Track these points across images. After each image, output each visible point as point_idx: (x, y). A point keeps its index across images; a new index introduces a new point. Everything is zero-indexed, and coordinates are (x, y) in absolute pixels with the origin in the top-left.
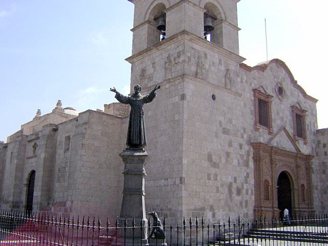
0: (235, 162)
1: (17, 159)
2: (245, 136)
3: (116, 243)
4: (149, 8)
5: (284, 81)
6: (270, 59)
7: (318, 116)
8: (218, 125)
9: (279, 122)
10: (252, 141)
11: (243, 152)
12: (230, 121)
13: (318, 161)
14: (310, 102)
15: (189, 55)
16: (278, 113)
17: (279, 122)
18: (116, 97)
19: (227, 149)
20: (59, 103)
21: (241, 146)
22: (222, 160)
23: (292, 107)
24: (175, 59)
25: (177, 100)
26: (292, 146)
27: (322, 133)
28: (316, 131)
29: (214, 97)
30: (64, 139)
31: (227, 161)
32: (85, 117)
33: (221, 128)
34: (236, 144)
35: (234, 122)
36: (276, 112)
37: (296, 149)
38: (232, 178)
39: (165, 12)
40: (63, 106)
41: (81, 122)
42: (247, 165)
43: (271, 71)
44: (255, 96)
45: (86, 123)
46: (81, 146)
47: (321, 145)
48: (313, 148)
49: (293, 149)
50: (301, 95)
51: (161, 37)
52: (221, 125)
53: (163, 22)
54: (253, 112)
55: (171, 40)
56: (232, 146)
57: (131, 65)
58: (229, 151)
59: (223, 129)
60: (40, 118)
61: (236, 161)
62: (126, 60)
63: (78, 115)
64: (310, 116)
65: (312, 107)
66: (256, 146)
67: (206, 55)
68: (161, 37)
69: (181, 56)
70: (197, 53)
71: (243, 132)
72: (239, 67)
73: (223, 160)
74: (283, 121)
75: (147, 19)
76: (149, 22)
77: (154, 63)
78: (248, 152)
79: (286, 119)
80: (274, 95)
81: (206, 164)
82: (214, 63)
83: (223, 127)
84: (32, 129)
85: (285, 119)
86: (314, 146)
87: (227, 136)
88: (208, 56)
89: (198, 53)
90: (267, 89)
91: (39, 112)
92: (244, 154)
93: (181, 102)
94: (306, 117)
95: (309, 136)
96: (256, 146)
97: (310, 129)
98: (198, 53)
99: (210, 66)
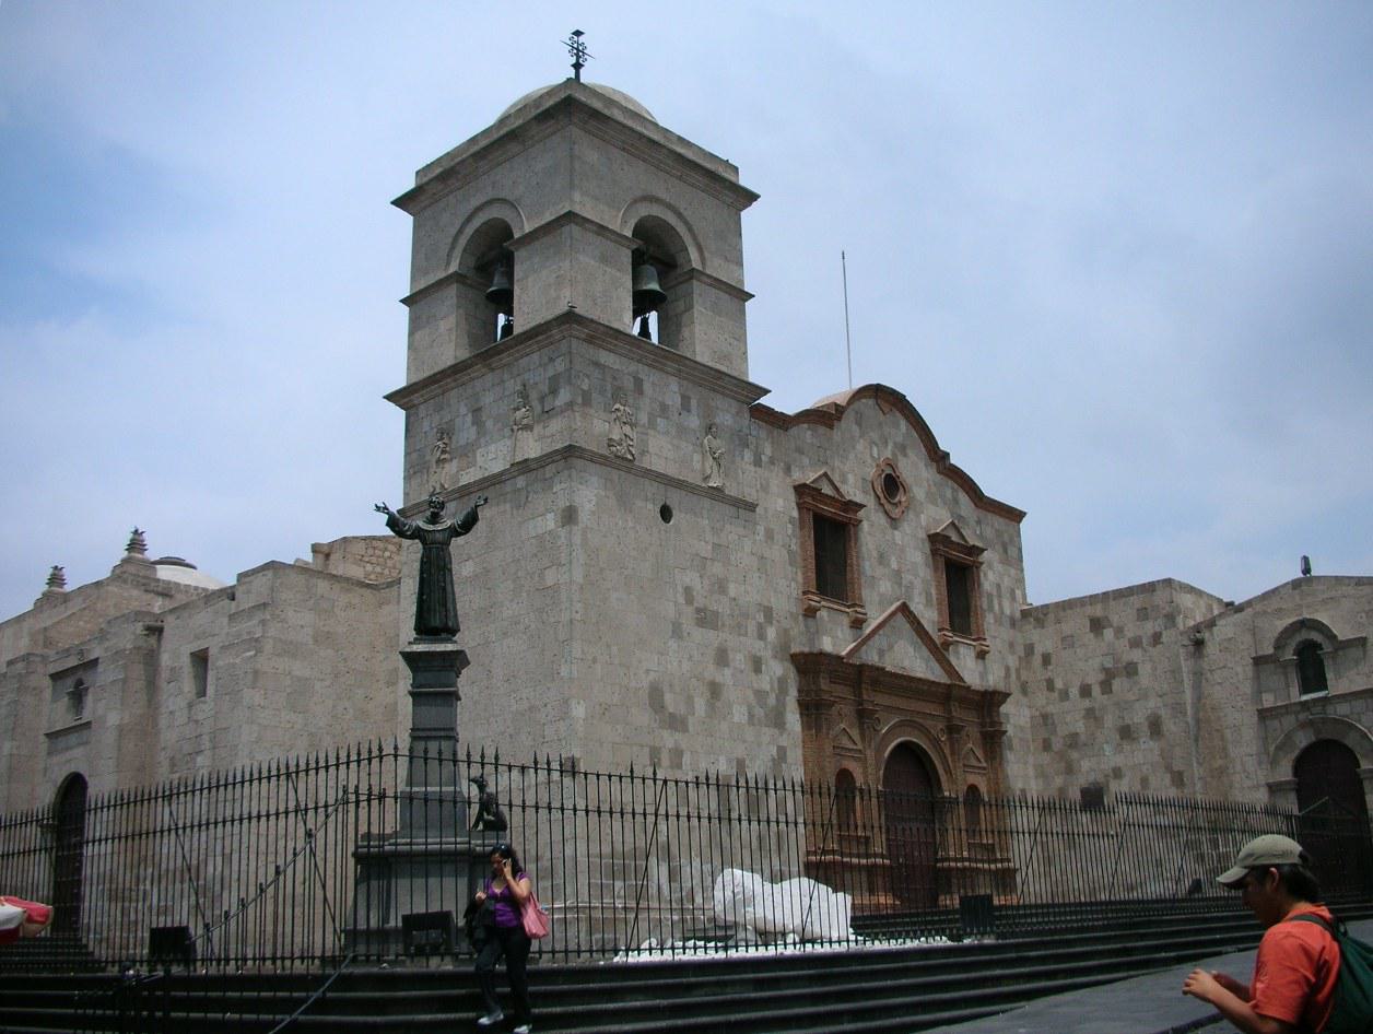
0: (739, 715)
2: (771, 633)
3: (426, 838)
4: (460, 231)
6: (859, 384)
7: (1026, 564)
8: (681, 600)
9: (885, 586)
10: (795, 649)
11: (765, 682)
12: (721, 586)
13: (1027, 712)
14: (998, 522)
15: (585, 387)
16: (882, 559)
17: (885, 586)
18: (387, 525)
19: (711, 672)
20: (136, 544)
21: (757, 665)
22: (697, 706)
23: (934, 539)
24: (542, 399)
25: (551, 525)
26: (936, 666)
27: (1037, 620)
30: (186, 661)
31: (711, 707)
32: (261, 583)
33: (690, 610)
34: (739, 656)
35: (732, 590)
36: (875, 554)
37: (947, 672)
38: (729, 761)
39: (512, 248)
40: (152, 554)
41: (245, 601)
42: (778, 722)
43: (859, 424)
44: (800, 506)
45: (265, 605)
46: (250, 677)
47: (1037, 660)
48: (1007, 669)
49: (934, 673)
50: (963, 498)
51: (502, 320)
52: (689, 600)
53: (505, 280)
54: (799, 559)
55: (531, 338)
56: (727, 665)
57: (403, 413)
58: (719, 679)
59: (698, 610)
60: (66, 597)
61: (744, 709)
62: (389, 397)
63: (233, 582)
65: (1006, 538)
66: (810, 665)
68: (502, 320)
69: (562, 391)
70: (609, 379)
71: (762, 620)
72: (747, 415)
73: (700, 705)
74: (900, 585)
75: (453, 268)
76: (457, 278)
77: (479, 409)
78: (782, 682)
79: (910, 577)
80: (870, 501)
81: (643, 717)
82: (664, 408)
83: (696, 605)
84: (41, 637)
85: (907, 578)
86: (1012, 661)
87: (712, 634)
88: (647, 386)
89: (614, 378)
90: (844, 481)
91: (56, 578)
92: (768, 688)
93: (562, 532)
94: (984, 567)
95: (996, 634)
96: (810, 665)
97: (996, 607)
98: (614, 378)
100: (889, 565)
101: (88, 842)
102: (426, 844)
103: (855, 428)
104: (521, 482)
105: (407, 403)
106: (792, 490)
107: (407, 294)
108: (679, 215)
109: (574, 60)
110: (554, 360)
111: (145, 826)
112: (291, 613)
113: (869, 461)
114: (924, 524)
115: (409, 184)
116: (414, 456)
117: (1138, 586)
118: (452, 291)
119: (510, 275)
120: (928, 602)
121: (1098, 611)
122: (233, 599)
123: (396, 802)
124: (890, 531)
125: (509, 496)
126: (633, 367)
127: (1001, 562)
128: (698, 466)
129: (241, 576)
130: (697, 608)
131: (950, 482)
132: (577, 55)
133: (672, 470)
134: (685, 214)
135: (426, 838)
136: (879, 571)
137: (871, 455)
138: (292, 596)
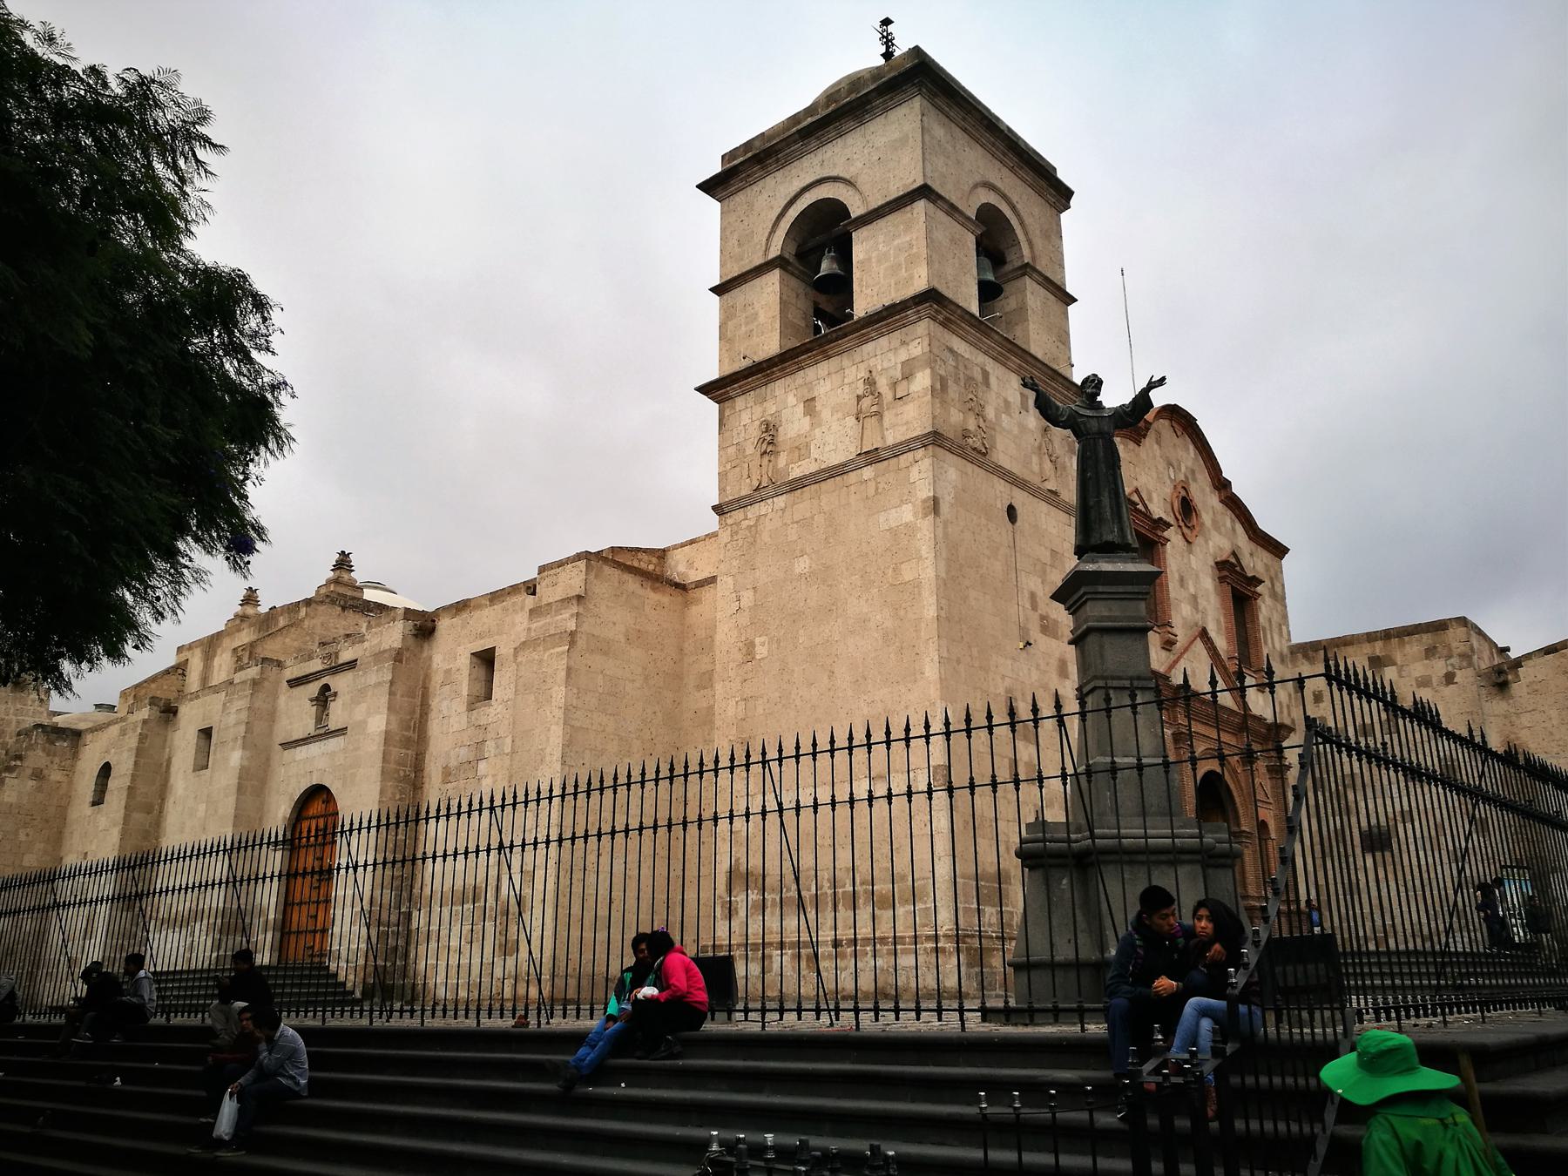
1: (244, 747)
3: (1044, 832)
5: (1195, 480)
8: (1028, 606)
20: (343, 563)
24: (894, 385)
28: (1286, 651)
29: (1011, 512)
30: (464, 661)
36: (1177, 576)
40: (359, 576)
43: (1158, 443)
50: (1239, 528)
59: (1043, 618)
64: (1268, 601)
67: (986, 375)
75: (774, 252)
76: (779, 263)
83: (1040, 612)
85: (1202, 602)
88: (993, 380)
90: (1150, 500)
99: (997, 416)
100: (1188, 589)
101: (284, 842)
102: (1173, 836)
103: (1156, 447)
104: (868, 472)
105: (721, 395)
106: (294, 690)
107: (717, 282)
108: (1013, 208)
109: (883, 49)
110: (908, 344)
111: (531, 816)
112: (603, 608)
113: (1168, 481)
114: (1211, 551)
115: (716, 168)
116: (732, 450)
117: (1363, 635)
118: (774, 278)
119: (845, 258)
120: (1219, 629)
121: (1378, 648)
122: (534, 593)
123: (1065, 784)
124: (1186, 554)
125: (852, 488)
126: (981, 358)
127: (1270, 596)
128: (1036, 468)
129: (542, 569)
130: (1041, 615)
131: (1229, 512)
132: (886, 43)
133: (1016, 469)
134: (1018, 206)
135: (1044, 832)
136: (1183, 594)
137: (1170, 477)
138: (604, 591)
